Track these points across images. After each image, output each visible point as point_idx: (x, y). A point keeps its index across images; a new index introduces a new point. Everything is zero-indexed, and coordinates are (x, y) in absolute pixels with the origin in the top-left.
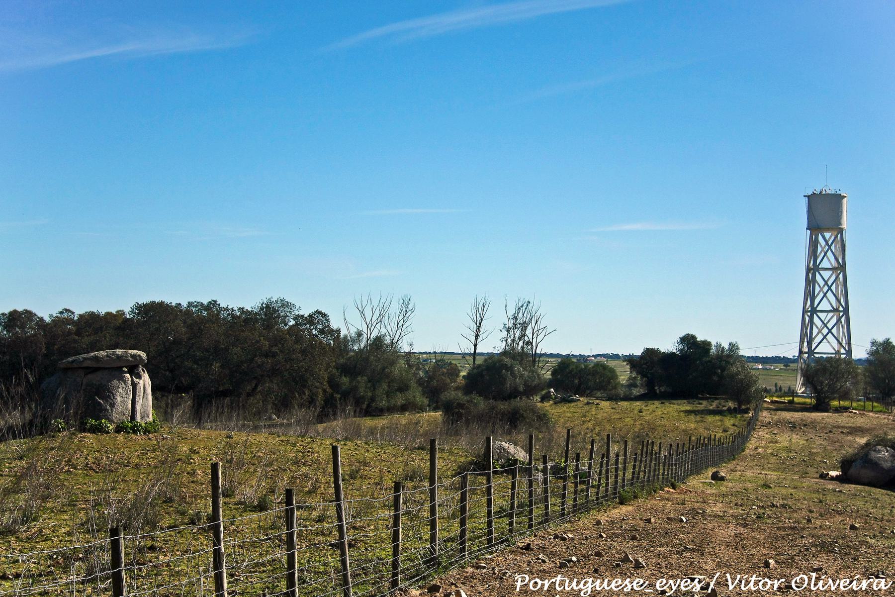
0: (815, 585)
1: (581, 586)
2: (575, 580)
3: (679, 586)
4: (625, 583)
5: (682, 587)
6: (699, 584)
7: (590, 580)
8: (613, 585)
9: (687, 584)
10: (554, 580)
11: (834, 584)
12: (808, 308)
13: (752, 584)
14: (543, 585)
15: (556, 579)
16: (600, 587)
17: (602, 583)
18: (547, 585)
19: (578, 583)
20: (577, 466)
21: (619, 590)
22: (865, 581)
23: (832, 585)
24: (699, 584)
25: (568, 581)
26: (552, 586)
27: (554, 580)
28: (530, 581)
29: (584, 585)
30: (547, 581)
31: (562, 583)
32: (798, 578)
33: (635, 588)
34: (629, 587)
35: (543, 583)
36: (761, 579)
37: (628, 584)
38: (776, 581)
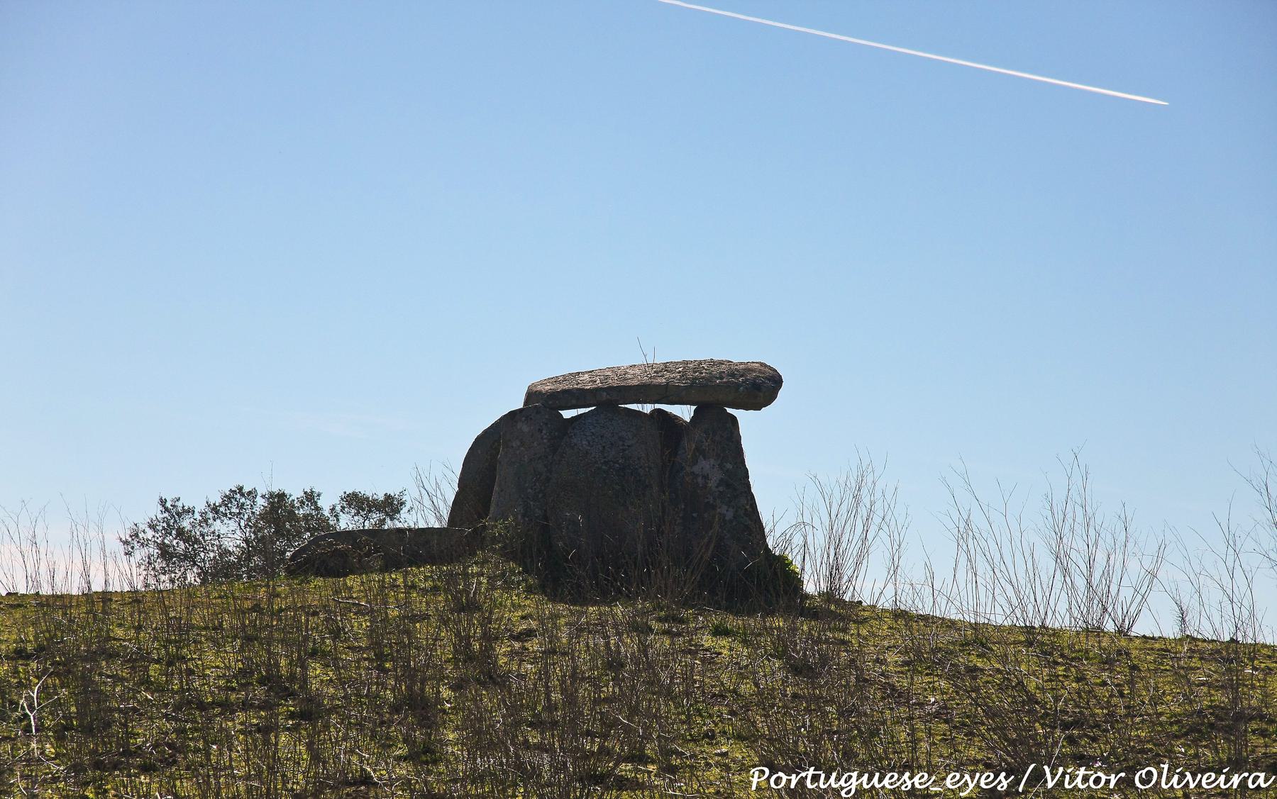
0: (1168, 780)
1: (842, 782)
2: (877, 775)
3: (1200, 781)
4: (904, 778)
5: (1204, 784)
6: (1006, 780)
7: (855, 775)
8: (886, 782)
9: (922, 780)
10: (803, 774)
11: (1194, 781)
12: (243, 695)
13: (1079, 780)
14: (1108, 782)
15: (807, 772)
16: (1225, 784)
17: (870, 780)
18: (794, 780)
19: (838, 779)
20: (757, 685)
21: (1145, 790)
22: (1237, 775)
23: (1191, 781)
24: (1006, 780)
25: (823, 776)
26: (802, 782)
27: (803, 774)
28: (768, 779)
29: (846, 782)
30: (1113, 776)
31: (815, 778)
32: (1144, 772)
33: (917, 786)
34: (909, 783)
35: (789, 778)
36: (1092, 772)
37: (907, 780)
38: (794, 775)
